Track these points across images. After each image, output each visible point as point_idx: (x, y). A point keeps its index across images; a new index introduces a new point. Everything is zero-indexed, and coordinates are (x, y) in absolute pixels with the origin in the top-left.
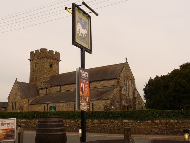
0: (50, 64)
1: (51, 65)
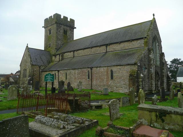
0: (64, 31)
1: (65, 33)
